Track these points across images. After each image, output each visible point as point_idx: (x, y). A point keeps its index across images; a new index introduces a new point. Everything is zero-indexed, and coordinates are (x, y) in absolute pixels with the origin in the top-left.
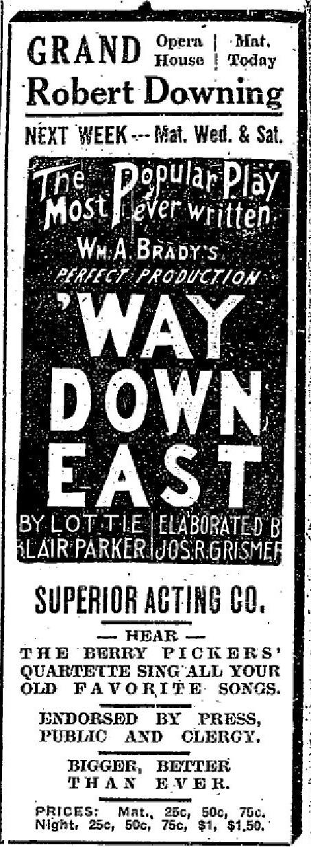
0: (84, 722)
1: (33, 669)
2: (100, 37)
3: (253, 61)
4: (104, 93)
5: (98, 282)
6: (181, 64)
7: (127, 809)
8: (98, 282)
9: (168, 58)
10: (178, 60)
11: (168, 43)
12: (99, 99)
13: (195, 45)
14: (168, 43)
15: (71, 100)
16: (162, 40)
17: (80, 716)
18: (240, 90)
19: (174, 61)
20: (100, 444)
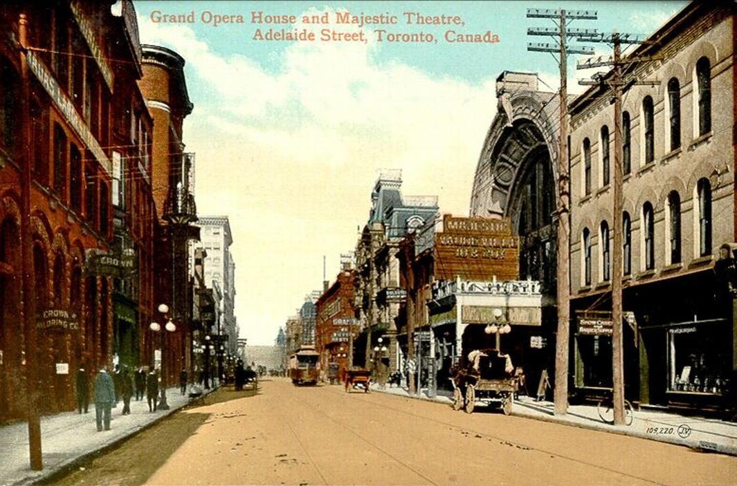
0: (450, 39)
1: (389, 21)
2: (337, 13)
3: (218, 19)
4: (350, 36)
5: (512, 126)
6: (184, 16)
7: (347, 14)
8: (512, 126)
9: (263, 16)
10: (320, 20)
11: (213, 18)
12: (226, 20)
13: (170, 21)
14: (213, 18)
15: (273, 21)
16: (207, 17)
17: (271, 21)
18: (362, 17)
19: (268, 19)
20: (170, 327)
